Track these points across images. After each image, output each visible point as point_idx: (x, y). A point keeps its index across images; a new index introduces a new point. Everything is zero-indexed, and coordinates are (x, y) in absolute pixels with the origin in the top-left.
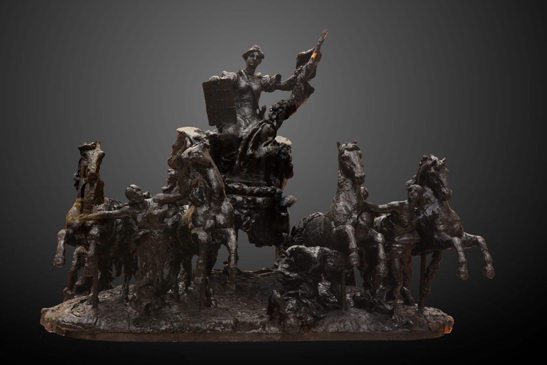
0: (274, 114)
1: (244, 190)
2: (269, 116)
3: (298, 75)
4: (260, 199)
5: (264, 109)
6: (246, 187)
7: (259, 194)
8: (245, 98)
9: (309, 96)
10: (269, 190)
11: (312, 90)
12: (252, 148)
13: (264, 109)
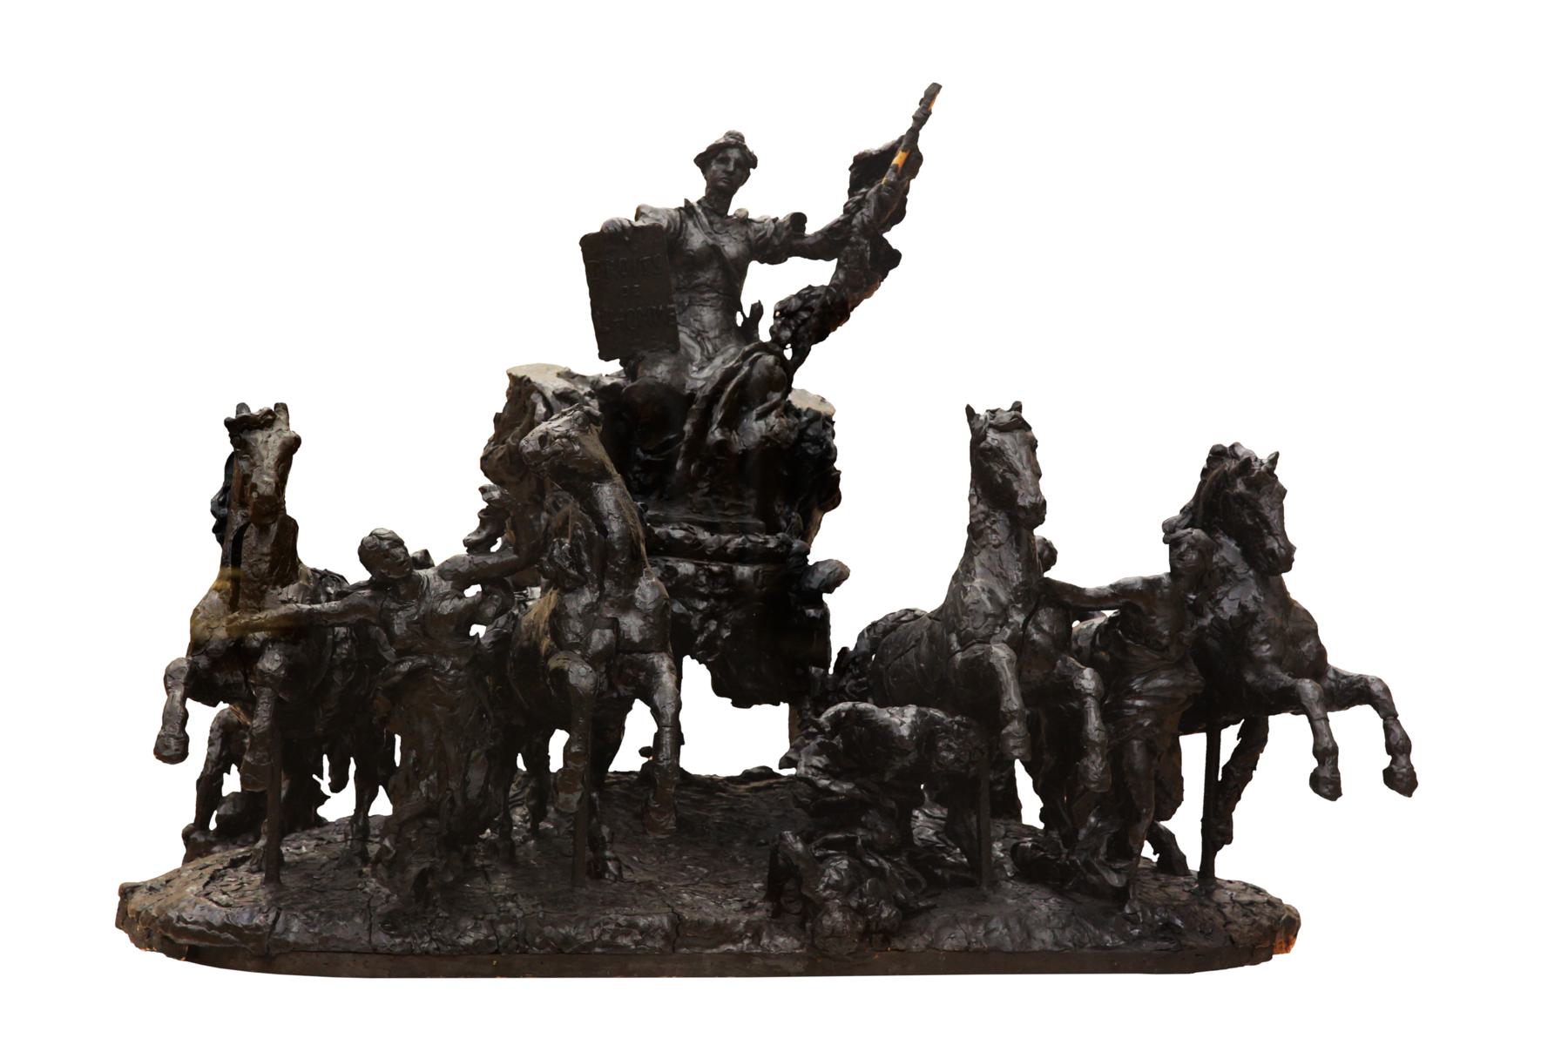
0: (784, 325)
1: (699, 543)
3: (853, 215)
4: (744, 571)
5: (757, 310)
6: (704, 536)
7: (742, 556)
9: (885, 275)
10: (771, 545)
12: (721, 425)
13: (757, 310)
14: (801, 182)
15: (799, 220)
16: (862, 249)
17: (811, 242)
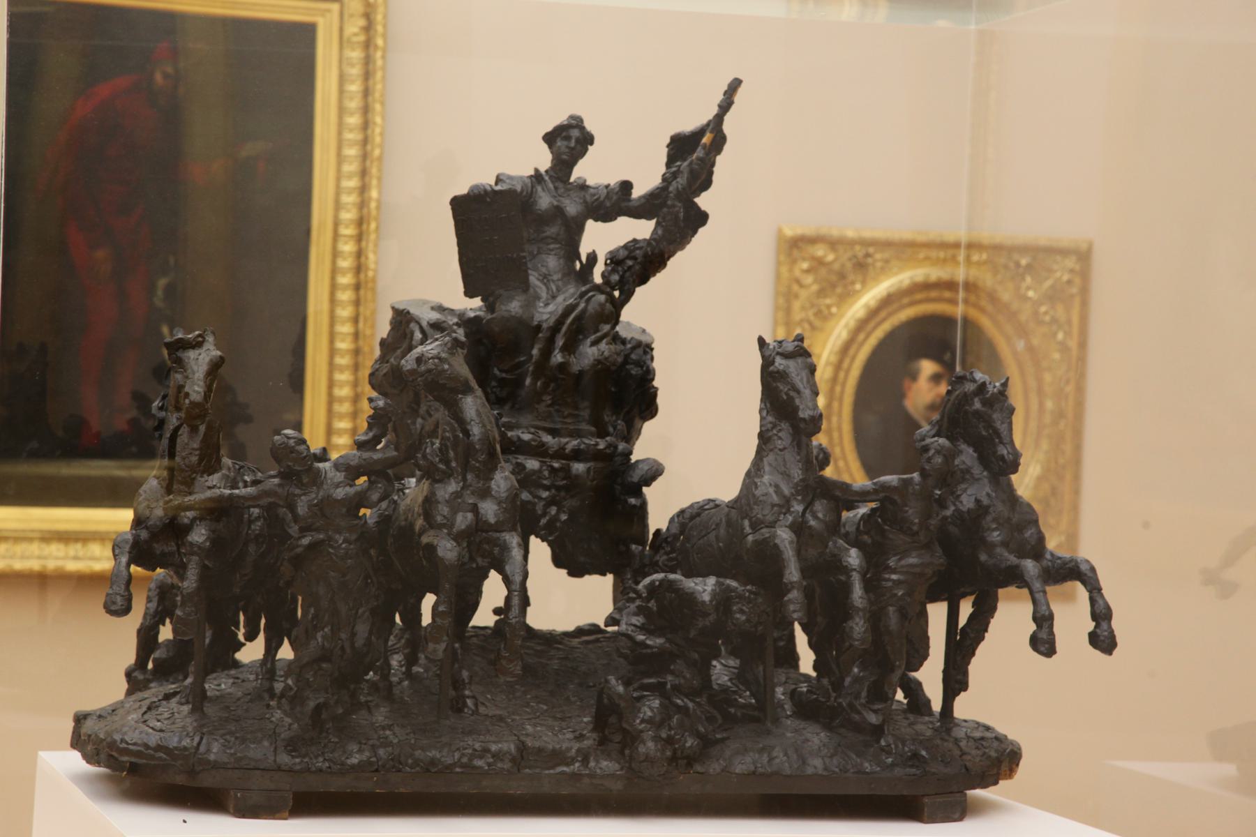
0: (614, 271)
1: (543, 444)
4: (579, 467)
5: (592, 258)
6: (547, 439)
7: (577, 455)
9: (695, 232)
11: (701, 218)
13: (592, 258)
14: (628, 156)
15: (626, 186)
16: (677, 210)
17: (637, 204)
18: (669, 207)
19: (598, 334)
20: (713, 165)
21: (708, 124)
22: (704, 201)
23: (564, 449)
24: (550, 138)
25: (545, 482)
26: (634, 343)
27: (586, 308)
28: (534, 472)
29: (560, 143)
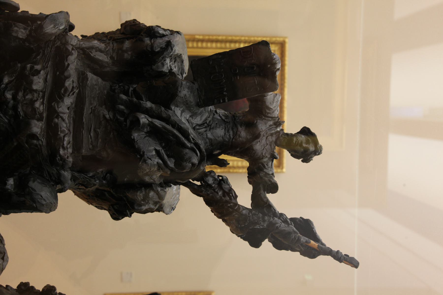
0: (215, 179)
1: (61, 98)
2: (211, 172)
3: (279, 218)
4: (37, 127)
5: (223, 164)
6: (68, 101)
7: (52, 130)
8: (240, 129)
9: (245, 239)
10: (61, 152)
11: (256, 244)
12: (151, 125)
13: (223, 164)
14: (295, 189)
15: (274, 188)
16: (260, 225)
17: (262, 196)
18: (263, 218)
19: (166, 157)
20: (293, 250)
21: (323, 244)
22: (267, 244)
23: (58, 117)
24: (306, 131)
25: (20, 94)
26: (162, 193)
27: (186, 147)
28: (31, 83)
29: (303, 138)
